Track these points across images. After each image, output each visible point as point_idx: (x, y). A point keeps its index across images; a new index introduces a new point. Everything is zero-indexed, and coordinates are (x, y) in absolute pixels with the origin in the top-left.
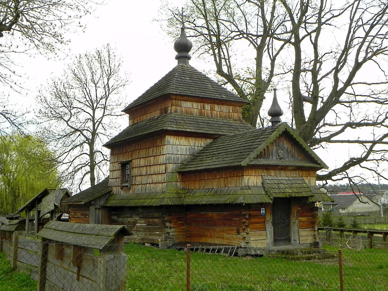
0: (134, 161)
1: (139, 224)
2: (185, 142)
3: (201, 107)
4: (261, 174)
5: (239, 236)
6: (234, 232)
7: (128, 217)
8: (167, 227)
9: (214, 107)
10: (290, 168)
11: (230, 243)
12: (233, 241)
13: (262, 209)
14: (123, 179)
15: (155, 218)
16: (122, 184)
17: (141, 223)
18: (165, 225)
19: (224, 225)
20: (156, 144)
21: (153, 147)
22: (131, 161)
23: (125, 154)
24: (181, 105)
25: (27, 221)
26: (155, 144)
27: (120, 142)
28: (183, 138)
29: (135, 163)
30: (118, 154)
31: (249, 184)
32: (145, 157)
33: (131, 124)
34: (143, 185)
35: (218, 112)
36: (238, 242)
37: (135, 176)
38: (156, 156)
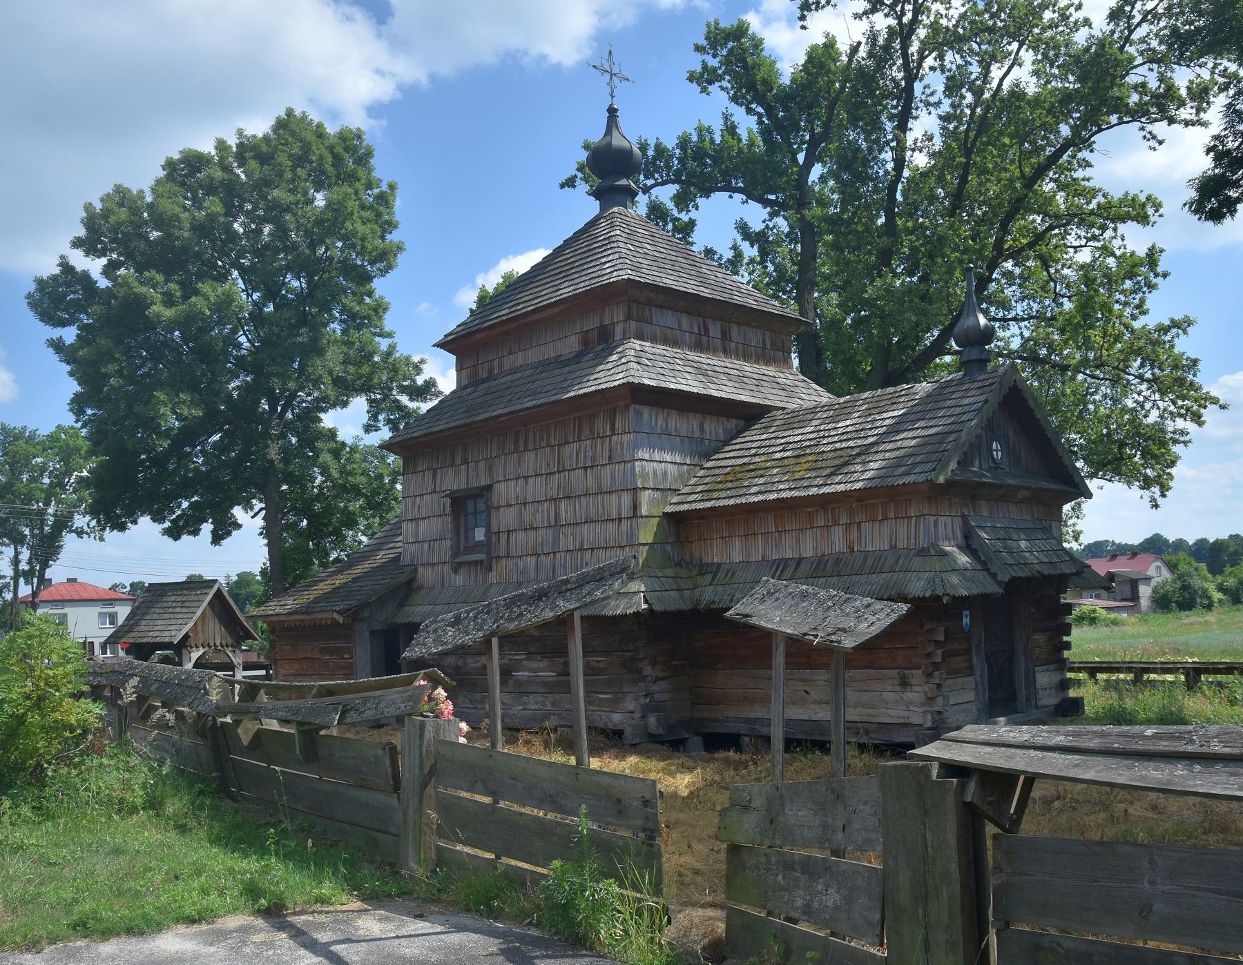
5: (909, 695)
10: (1021, 494)
12: (884, 711)
22: (489, 488)
24: (652, 321)
25: (778, 743)
27: (443, 434)
28: (674, 412)
29: (505, 491)
33: (463, 384)
34: (543, 558)
35: (741, 346)
36: (907, 713)
37: (509, 532)
38: (592, 467)
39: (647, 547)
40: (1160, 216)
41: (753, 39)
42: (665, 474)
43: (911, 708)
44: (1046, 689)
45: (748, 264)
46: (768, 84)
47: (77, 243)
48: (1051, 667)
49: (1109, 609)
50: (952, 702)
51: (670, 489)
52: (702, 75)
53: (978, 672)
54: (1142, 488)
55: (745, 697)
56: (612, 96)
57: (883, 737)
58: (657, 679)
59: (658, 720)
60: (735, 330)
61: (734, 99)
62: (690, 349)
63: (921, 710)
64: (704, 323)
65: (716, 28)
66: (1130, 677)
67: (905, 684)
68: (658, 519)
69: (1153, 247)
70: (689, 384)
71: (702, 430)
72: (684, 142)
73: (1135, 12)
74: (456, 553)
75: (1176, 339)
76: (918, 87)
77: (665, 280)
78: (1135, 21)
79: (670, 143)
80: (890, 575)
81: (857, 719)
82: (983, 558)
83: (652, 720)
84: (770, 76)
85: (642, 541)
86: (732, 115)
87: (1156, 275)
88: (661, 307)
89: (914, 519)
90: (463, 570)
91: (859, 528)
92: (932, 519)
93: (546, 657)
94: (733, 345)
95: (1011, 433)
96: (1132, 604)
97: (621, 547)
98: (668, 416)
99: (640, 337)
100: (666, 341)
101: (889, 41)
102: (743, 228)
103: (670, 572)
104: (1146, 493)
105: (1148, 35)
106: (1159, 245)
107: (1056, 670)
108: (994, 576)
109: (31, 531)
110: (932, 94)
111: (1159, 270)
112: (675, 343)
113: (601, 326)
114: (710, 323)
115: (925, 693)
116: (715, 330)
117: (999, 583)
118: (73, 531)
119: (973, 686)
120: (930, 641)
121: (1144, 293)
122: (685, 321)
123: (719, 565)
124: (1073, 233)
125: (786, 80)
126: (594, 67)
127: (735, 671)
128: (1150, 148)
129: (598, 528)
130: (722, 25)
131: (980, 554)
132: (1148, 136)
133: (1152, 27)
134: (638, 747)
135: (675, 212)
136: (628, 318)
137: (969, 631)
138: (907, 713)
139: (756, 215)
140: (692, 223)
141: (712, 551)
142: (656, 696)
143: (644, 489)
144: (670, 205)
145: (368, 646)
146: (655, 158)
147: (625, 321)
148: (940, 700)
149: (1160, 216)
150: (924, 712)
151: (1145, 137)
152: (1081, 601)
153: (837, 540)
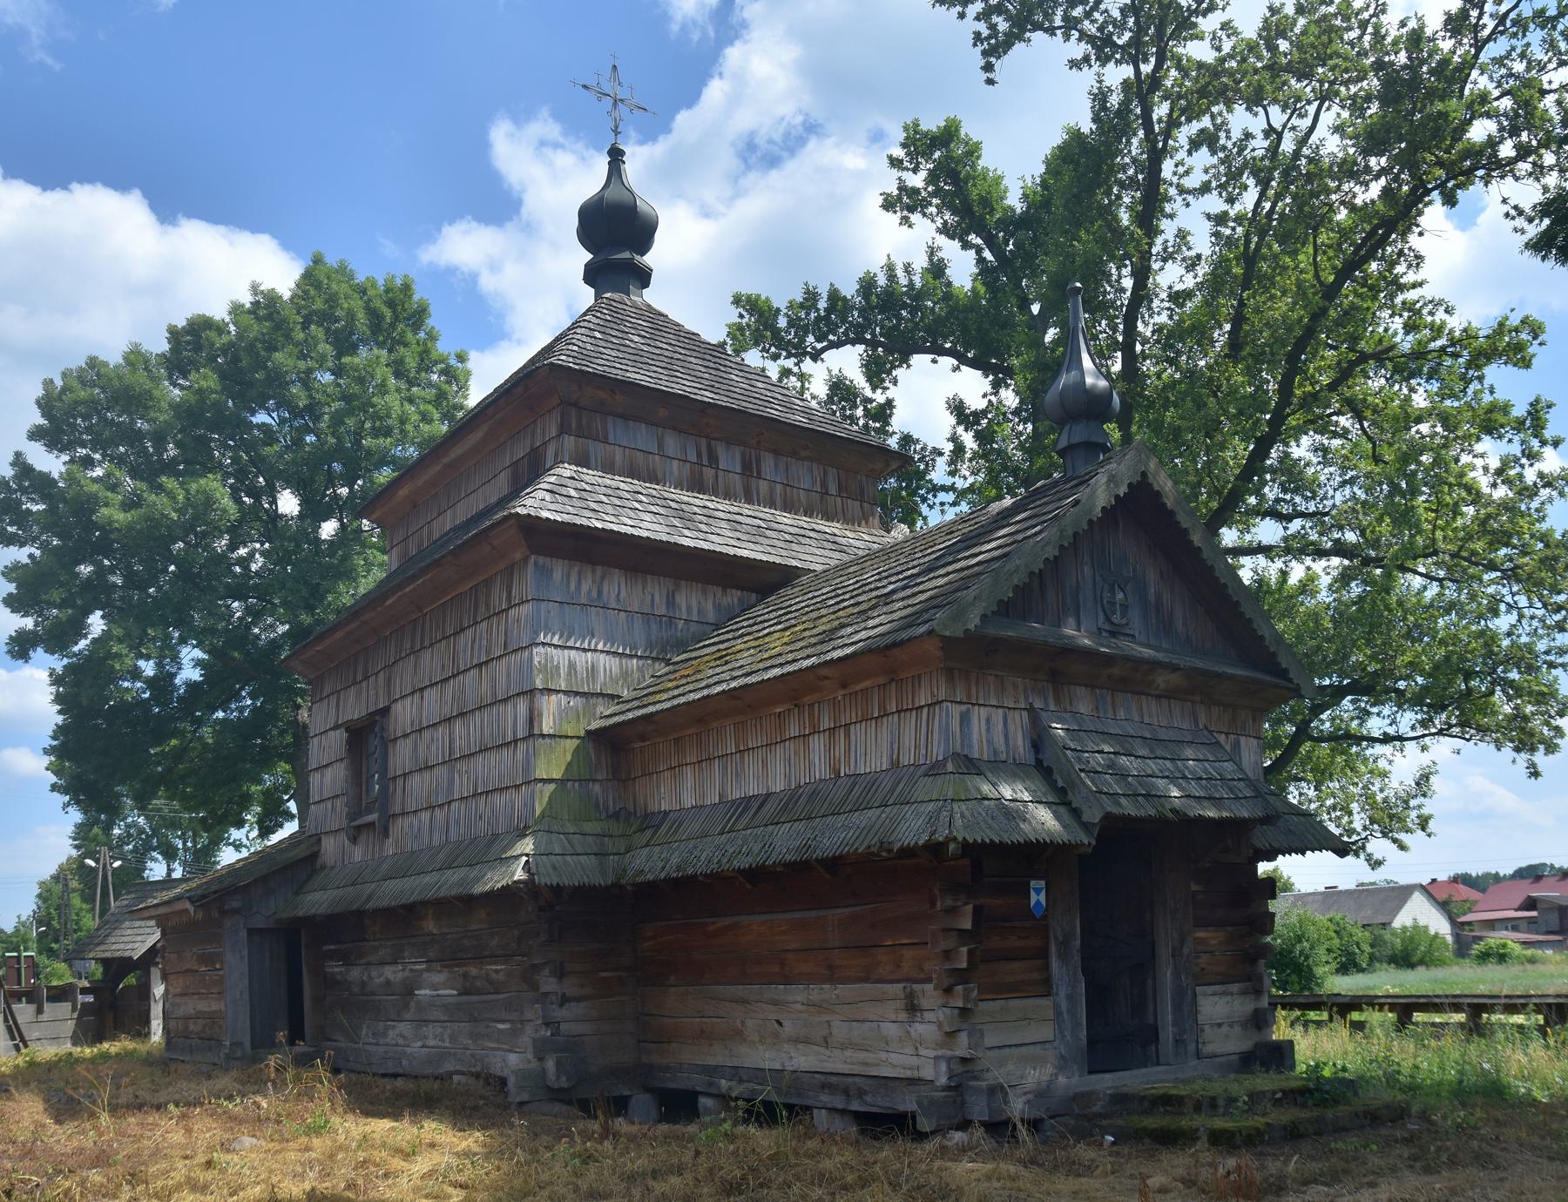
0: (398, 708)
1: (427, 992)
2: (623, 594)
3: (699, 455)
4: (1026, 698)
5: (919, 1029)
6: (894, 1009)
7: (382, 964)
8: (546, 994)
9: (758, 461)
10: (1162, 680)
11: (866, 1064)
12: (883, 1055)
13: (1033, 883)
14: (360, 798)
15: (494, 958)
16: (354, 820)
17: (436, 987)
18: (534, 987)
19: (832, 975)
20: (488, 606)
21: (476, 623)
22: (385, 712)
23: (364, 684)
26: (482, 608)
29: (404, 714)
30: (339, 692)
31: (971, 746)
32: (442, 681)
35: (779, 488)
36: (914, 1061)
37: (405, 775)
38: (486, 663)
39: (552, 786)
40: (1540, 344)
41: (967, 143)
42: (593, 671)
43: (923, 1052)
44: (1220, 1025)
45: (971, 460)
46: (987, 203)
47: (36, 434)
48: (1235, 987)
49: (1526, 944)
50: (990, 1040)
51: (602, 695)
52: (899, 198)
53: (1063, 992)
54: (1517, 750)
55: (702, 1031)
56: (616, 132)
57: (877, 1103)
58: (564, 1000)
59: (558, 1064)
60: (768, 463)
61: (945, 230)
62: (679, 485)
63: (932, 1054)
64: (709, 448)
65: (916, 132)
66: (1460, 1017)
67: (913, 1008)
68: (576, 742)
69: (1537, 401)
70: (648, 525)
71: (671, 602)
72: (867, 284)
73: (1486, 19)
74: (352, 816)
75: (1549, 506)
76: (1167, 168)
77: (628, 375)
78: (1486, 32)
79: (849, 289)
80: (878, 811)
81: (845, 1069)
82: (1060, 783)
83: (550, 1065)
84: (989, 193)
85: (541, 773)
86: (940, 248)
87: (1544, 443)
88: (625, 417)
89: (925, 710)
90: (363, 838)
91: (848, 735)
92: (956, 710)
93: (445, 967)
94: (763, 485)
95: (1152, 577)
96: (1560, 938)
97: (517, 787)
98: (603, 578)
99: (582, 461)
100: (632, 472)
101: (1125, 104)
102: (958, 408)
103: (592, 827)
104: (1523, 757)
105: (1509, 53)
106: (1546, 397)
107: (1244, 993)
108: (1076, 813)
109: (184, 843)
110: (1187, 173)
111: (1548, 434)
112: (652, 477)
113: (533, 450)
114: (720, 450)
115: (940, 1025)
116: (730, 459)
117: (1086, 826)
118: (230, 844)
119: (1051, 1014)
120: (945, 930)
121: (1522, 466)
122: (672, 443)
123: (666, 813)
124: (1421, 390)
125: (1014, 201)
126: (585, 87)
127: (691, 989)
128: (1516, 230)
129: (493, 757)
130: (924, 127)
131: (1056, 776)
132: (1513, 212)
133: (1514, 41)
134: (525, 1108)
135: (868, 393)
136: (563, 430)
137: (1045, 917)
138: (914, 1061)
139: (973, 387)
140: (889, 403)
141: (658, 786)
142: (563, 1027)
143: (550, 691)
144: (859, 380)
145: (245, 952)
146: (828, 311)
147: (558, 436)
148: (963, 1038)
149: (1540, 344)
150: (936, 1058)
151: (1507, 215)
152: (1492, 934)
153: (815, 761)
